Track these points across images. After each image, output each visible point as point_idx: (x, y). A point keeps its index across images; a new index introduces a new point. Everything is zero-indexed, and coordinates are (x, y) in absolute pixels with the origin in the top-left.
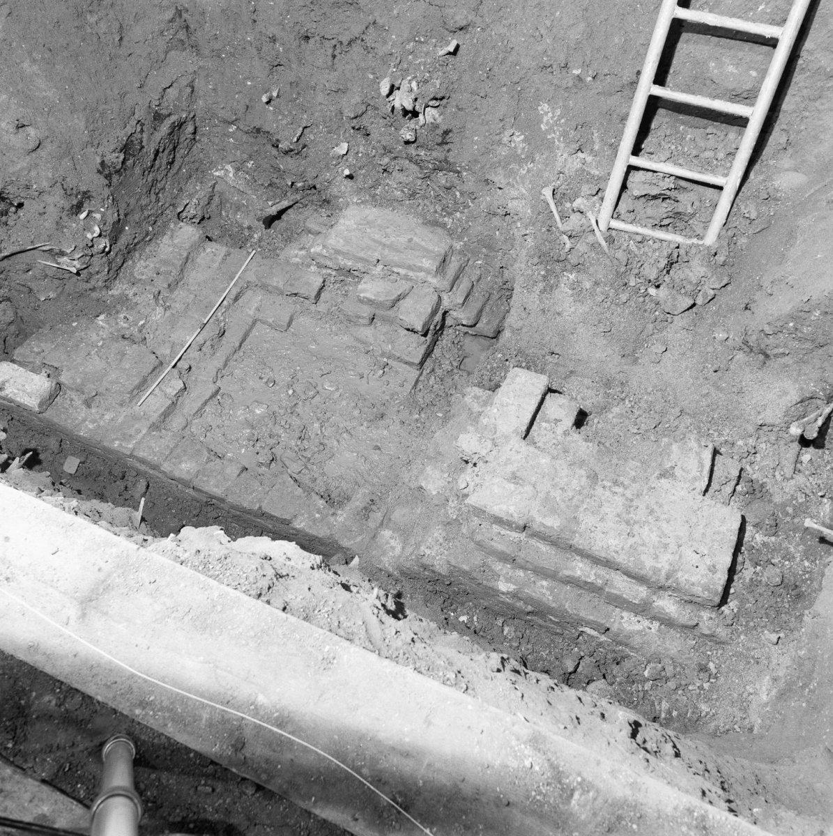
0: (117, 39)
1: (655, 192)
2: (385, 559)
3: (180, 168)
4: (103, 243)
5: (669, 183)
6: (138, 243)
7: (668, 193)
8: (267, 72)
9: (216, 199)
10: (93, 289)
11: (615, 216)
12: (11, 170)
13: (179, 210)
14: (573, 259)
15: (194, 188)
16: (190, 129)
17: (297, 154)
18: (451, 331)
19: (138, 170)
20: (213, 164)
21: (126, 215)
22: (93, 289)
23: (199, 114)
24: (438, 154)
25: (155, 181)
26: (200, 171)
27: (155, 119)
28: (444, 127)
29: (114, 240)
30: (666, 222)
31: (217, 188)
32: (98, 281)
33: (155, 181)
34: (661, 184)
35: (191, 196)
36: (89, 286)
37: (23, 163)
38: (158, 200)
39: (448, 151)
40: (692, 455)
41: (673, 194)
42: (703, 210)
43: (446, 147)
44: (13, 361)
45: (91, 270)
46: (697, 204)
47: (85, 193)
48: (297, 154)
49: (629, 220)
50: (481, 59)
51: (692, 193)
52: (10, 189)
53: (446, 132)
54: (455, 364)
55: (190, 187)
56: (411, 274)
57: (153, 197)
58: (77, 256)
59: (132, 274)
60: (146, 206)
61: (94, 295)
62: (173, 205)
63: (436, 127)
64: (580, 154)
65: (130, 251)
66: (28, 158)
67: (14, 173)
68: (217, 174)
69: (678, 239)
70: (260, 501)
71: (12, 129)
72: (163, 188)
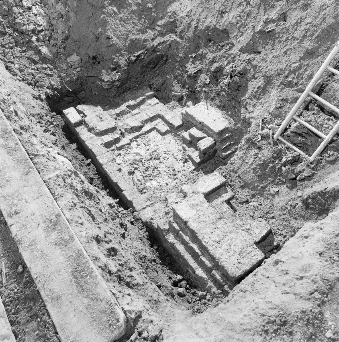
0: (151, 22)
1: (299, 132)
2: (143, 216)
3: (156, 70)
4: (118, 83)
5: (305, 131)
6: (130, 88)
7: (304, 134)
8: (194, 48)
9: (165, 85)
10: (109, 97)
11: (282, 135)
12: (101, 50)
13: (150, 84)
14: (259, 144)
15: (159, 78)
16: (165, 59)
17: (193, 78)
18: (217, 158)
19: (140, 65)
20: (168, 73)
21: (130, 78)
22: (109, 97)
23: (170, 55)
24: (235, 93)
25: (145, 72)
26: (163, 74)
27: (153, 51)
28: (239, 84)
29: (122, 84)
30: (300, 145)
31: (166, 82)
32: (112, 94)
33: (145, 72)
34: (302, 130)
35: (156, 81)
36: (108, 95)
37: (104, 49)
38: (144, 78)
39: (238, 93)
40: (260, 228)
41: (306, 135)
42: (315, 145)
43: (238, 92)
44: (75, 108)
45: (111, 90)
46: (313, 142)
47: (119, 65)
48: (193, 78)
49: (286, 139)
50: (260, 65)
51: (313, 138)
52: (98, 56)
53: (239, 86)
54: (211, 170)
55: (157, 78)
56: (209, 131)
57: (142, 76)
58: (107, 84)
59: (124, 97)
60: (139, 78)
61: (109, 98)
62: (149, 81)
63: (237, 83)
64: (280, 109)
65: (126, 90)
66: (106, 48)
67: (100, 52)
68: (168, 77)
69: (302, 153)
70: (119, 181)
71: (105, 38)
72: (148, 75)
